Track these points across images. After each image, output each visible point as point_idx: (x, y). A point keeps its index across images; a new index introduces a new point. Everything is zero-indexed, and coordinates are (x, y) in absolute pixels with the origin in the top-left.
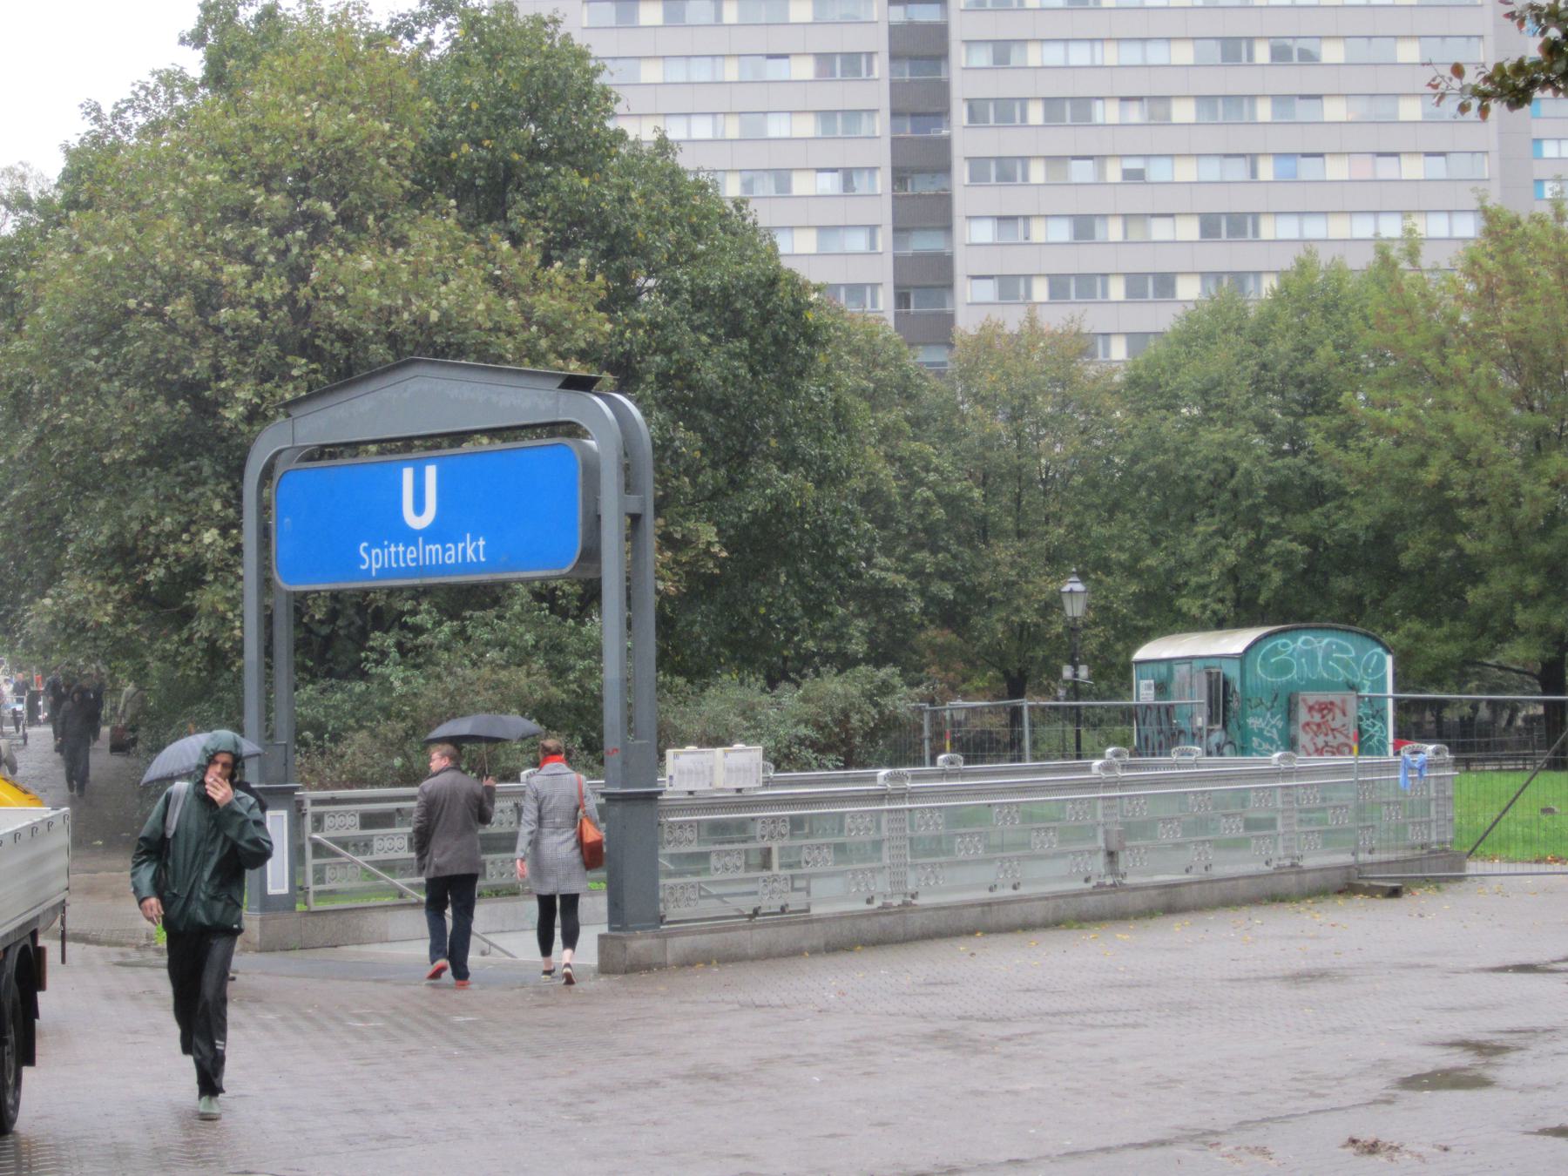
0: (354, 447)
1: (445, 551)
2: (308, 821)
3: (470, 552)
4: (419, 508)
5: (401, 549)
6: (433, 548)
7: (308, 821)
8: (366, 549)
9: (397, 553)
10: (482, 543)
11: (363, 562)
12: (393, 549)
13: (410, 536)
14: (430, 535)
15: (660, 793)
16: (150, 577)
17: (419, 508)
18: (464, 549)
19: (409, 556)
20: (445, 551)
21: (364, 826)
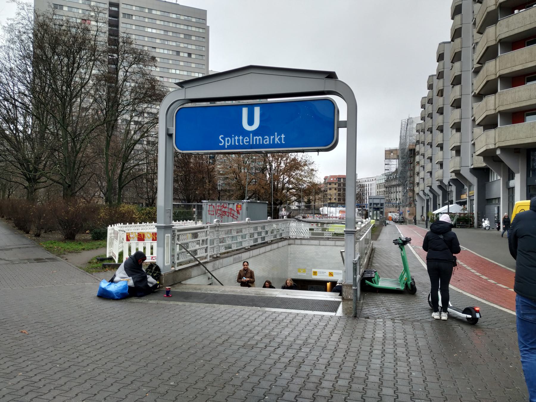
0: (403, 258)
1: (263, 139)
2: (176, 237)
3: (277, 139)
4: (251, 122)
5: (241, 138)
6: (258, 138)
7: (176, 237)
8: (222, 138)
9: (239, 140)
10: (283, 136)
11: (221, 142)
12: (237, 138)
13: (246, 133)
14: (255, 133)
15: (173, 226)
16: (222, 182)
17: (251, 122)
18: (274, 139)
19: (245, 141)
20: (263, 139)
21: (322, 230)
